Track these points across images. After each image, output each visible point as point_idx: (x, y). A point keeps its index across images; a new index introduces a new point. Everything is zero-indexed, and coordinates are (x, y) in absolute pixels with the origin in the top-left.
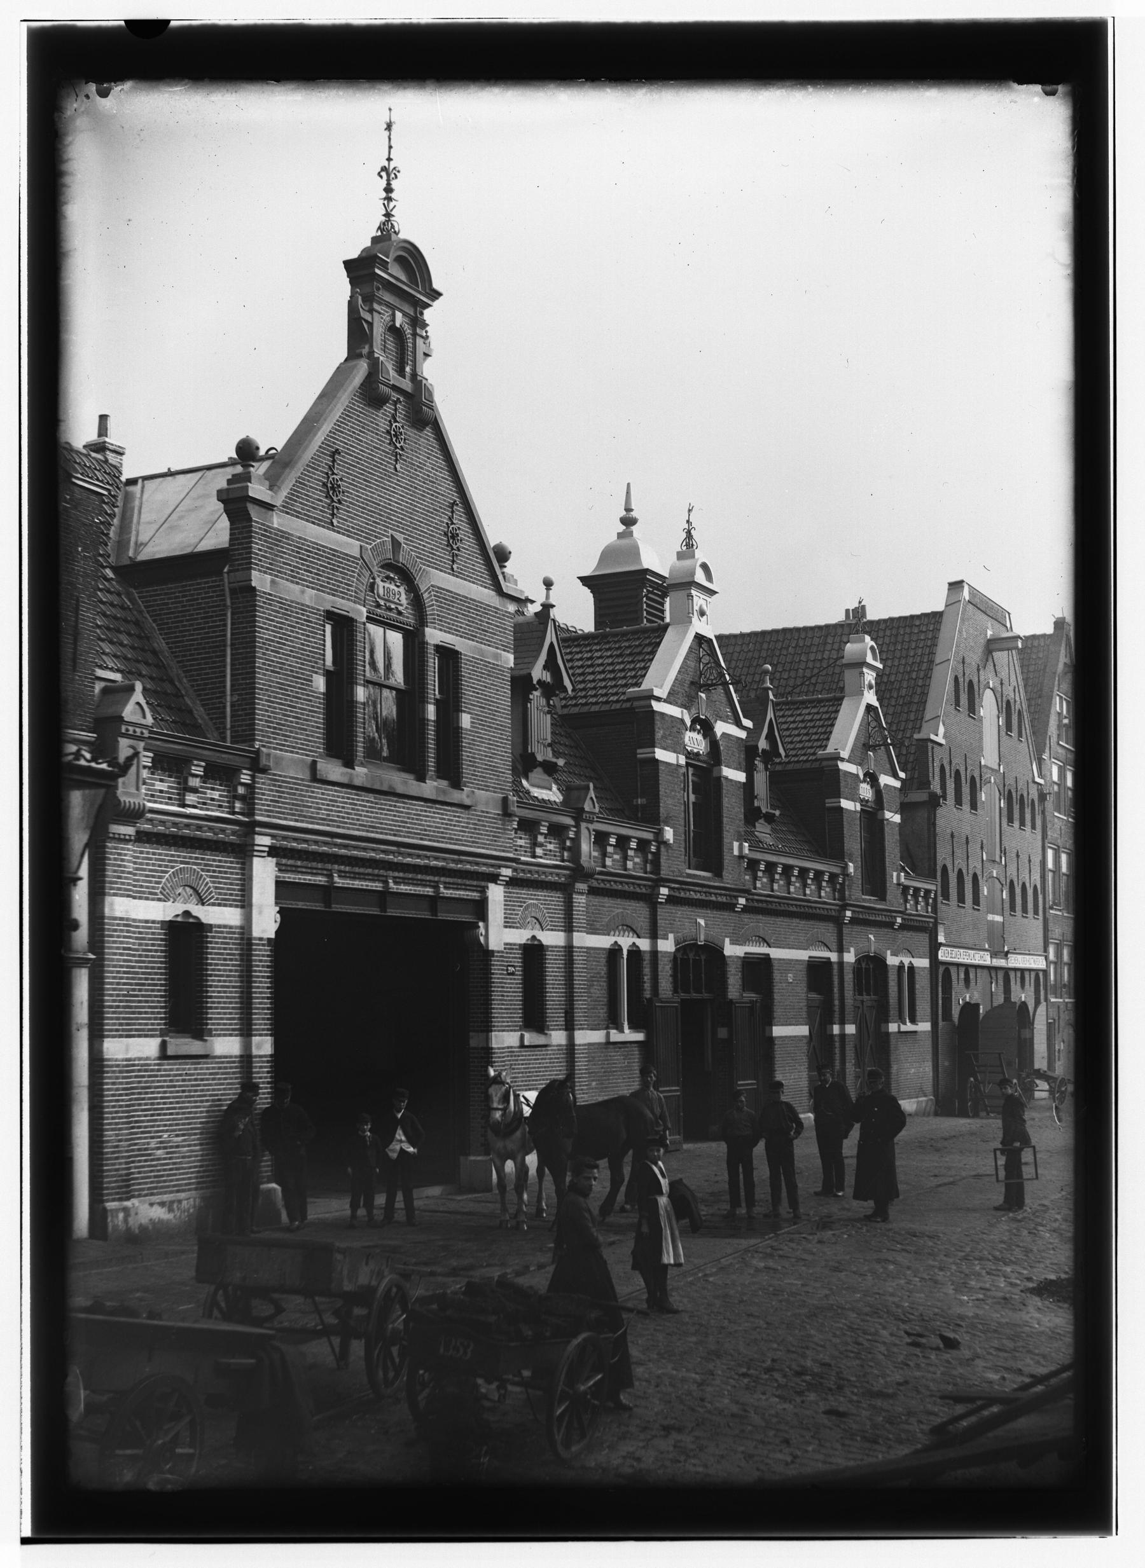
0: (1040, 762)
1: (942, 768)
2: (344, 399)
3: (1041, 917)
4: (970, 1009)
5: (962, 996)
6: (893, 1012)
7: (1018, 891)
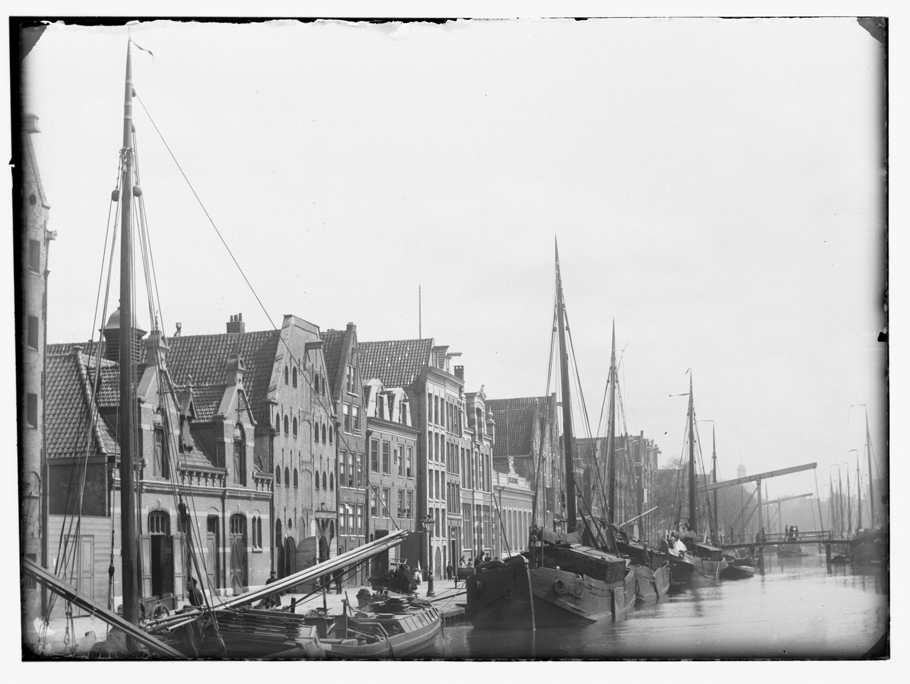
0: (335, 405)
1: (278, 415)
2: (643, 612)
3: (275, 520)
4: (290, 540)
5: (286, 533)
6: (250, 541)
7: (321, 477)
